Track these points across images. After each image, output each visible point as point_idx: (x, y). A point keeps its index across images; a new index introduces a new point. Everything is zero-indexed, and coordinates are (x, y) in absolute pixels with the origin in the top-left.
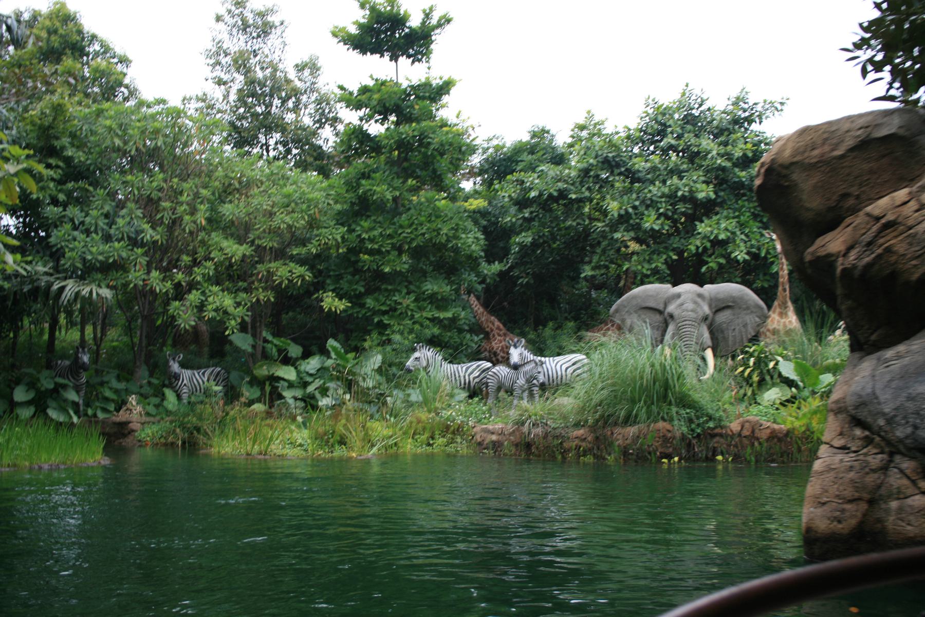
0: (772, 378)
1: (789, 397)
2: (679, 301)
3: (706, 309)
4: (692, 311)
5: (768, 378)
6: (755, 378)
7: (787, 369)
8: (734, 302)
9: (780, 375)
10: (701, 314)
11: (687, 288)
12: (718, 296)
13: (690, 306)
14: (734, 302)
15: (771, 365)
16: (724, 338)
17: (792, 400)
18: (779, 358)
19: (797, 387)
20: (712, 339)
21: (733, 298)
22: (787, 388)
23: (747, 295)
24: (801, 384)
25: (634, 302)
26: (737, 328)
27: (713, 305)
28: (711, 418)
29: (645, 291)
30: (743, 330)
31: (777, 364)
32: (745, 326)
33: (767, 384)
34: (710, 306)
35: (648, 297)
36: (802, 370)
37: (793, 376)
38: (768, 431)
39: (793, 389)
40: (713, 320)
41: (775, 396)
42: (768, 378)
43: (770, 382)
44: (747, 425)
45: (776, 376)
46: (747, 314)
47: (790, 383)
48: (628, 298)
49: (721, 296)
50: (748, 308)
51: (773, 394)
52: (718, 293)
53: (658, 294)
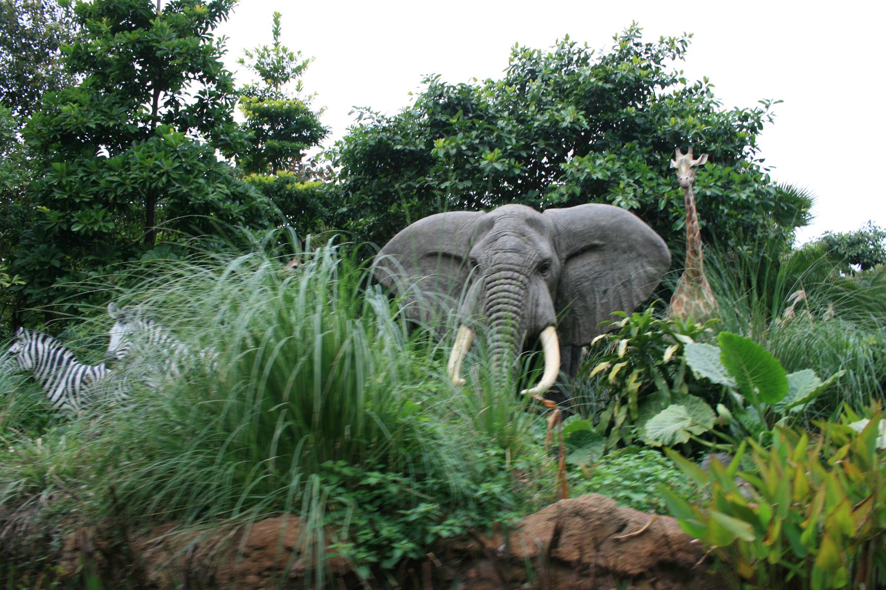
0: (670, 384)
1: (710, 426)
2: (489, 235)
3: (545, 248)
4: (515, 250)
5: (661, 384)
6: (633, 384)
7: (706, 361)
8: (601, 238)
9: (689, 376)
10: (533, 257)
11: (510, 213)
12: (572, 227)
13: (511, 241)
14: (601, 238)
15: (668, 354)
16: (586, 308)
17: (721, 433)
18: (685, 339)
19: (729, 402)
20: (558, 307)
21: (602, 229)
22: (706, 407)
23: (627, 222)
24: (738, 397)
25: (414, 246)
26: (612, 288)
27: (563, 245)
28: (450, 501)
29: (434, 223)
30: (623, 291)
31: (680, 352)
32: (627, 283)
33: (659, 398)
34: (555, 246)
35: (448, 233)
36: (741, 357)
37: (719, 375)
38: (647, 546)
39: (721, 408)
40: (562, 273)
41: (677, 426)
42: (661, 384)
43: (666, 393)
44: (575, 526)
45: (679, 379)
46: (629, 260)
47: (710, 393)
48: (407, 232)
49: (579, 227)
50: (631, 248)
51: (670, 422)
52: (573, 222)
53: (457, 228)
